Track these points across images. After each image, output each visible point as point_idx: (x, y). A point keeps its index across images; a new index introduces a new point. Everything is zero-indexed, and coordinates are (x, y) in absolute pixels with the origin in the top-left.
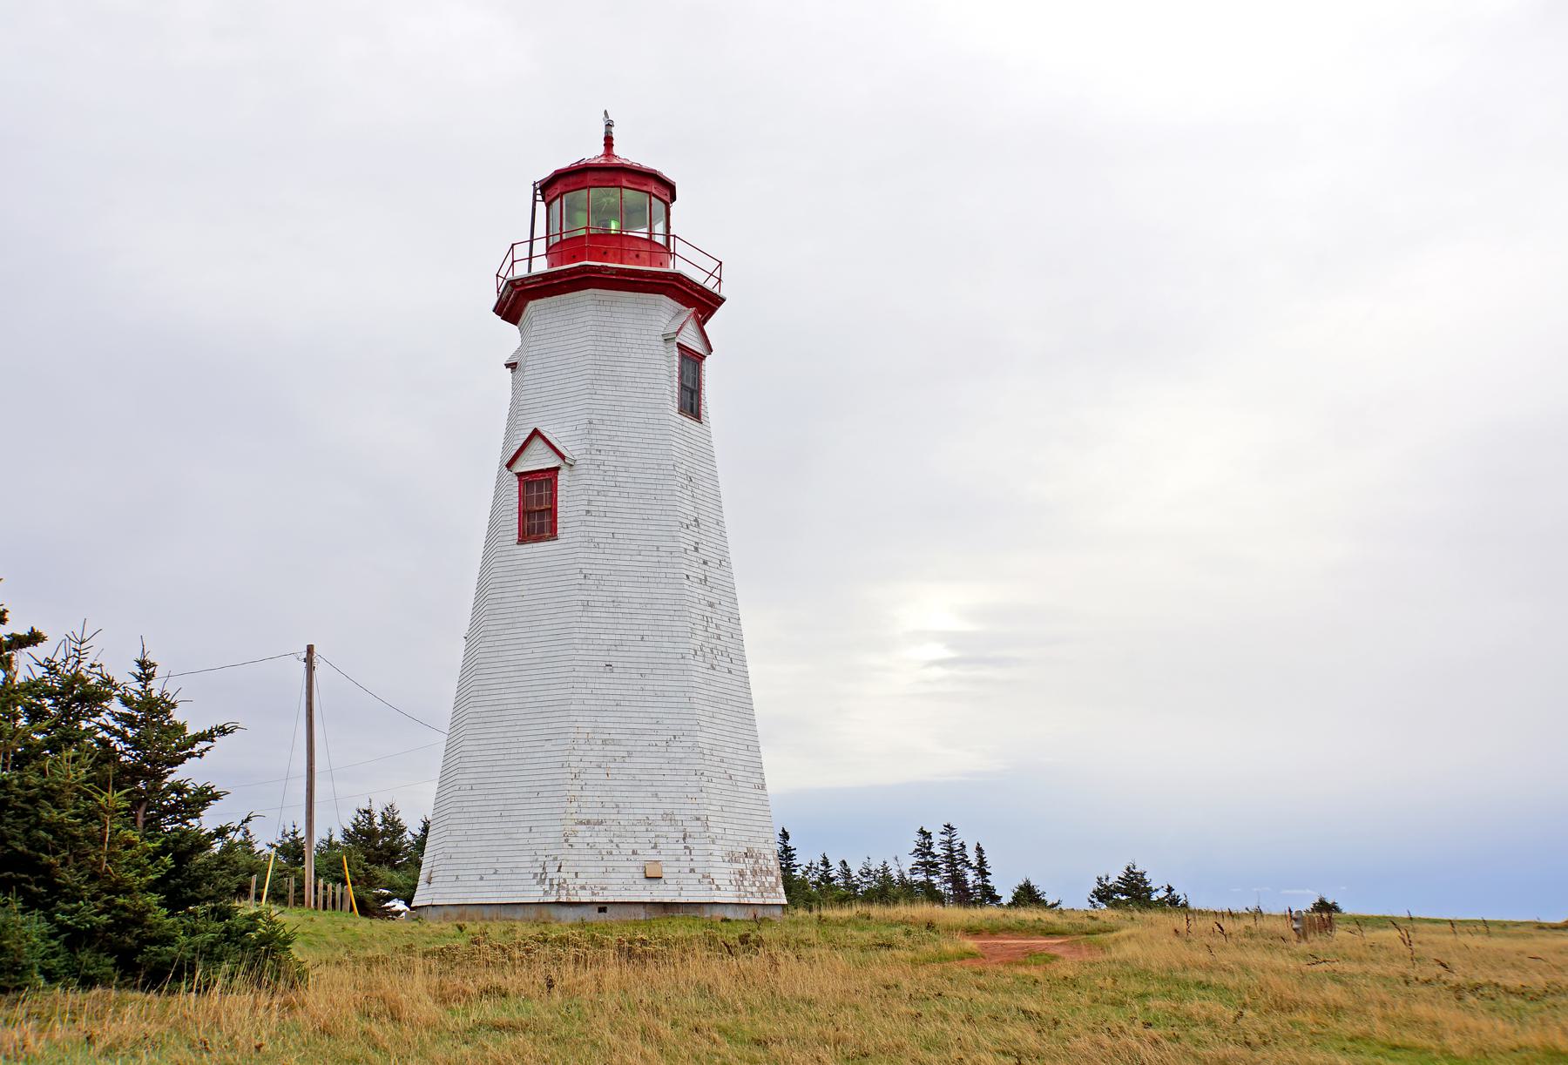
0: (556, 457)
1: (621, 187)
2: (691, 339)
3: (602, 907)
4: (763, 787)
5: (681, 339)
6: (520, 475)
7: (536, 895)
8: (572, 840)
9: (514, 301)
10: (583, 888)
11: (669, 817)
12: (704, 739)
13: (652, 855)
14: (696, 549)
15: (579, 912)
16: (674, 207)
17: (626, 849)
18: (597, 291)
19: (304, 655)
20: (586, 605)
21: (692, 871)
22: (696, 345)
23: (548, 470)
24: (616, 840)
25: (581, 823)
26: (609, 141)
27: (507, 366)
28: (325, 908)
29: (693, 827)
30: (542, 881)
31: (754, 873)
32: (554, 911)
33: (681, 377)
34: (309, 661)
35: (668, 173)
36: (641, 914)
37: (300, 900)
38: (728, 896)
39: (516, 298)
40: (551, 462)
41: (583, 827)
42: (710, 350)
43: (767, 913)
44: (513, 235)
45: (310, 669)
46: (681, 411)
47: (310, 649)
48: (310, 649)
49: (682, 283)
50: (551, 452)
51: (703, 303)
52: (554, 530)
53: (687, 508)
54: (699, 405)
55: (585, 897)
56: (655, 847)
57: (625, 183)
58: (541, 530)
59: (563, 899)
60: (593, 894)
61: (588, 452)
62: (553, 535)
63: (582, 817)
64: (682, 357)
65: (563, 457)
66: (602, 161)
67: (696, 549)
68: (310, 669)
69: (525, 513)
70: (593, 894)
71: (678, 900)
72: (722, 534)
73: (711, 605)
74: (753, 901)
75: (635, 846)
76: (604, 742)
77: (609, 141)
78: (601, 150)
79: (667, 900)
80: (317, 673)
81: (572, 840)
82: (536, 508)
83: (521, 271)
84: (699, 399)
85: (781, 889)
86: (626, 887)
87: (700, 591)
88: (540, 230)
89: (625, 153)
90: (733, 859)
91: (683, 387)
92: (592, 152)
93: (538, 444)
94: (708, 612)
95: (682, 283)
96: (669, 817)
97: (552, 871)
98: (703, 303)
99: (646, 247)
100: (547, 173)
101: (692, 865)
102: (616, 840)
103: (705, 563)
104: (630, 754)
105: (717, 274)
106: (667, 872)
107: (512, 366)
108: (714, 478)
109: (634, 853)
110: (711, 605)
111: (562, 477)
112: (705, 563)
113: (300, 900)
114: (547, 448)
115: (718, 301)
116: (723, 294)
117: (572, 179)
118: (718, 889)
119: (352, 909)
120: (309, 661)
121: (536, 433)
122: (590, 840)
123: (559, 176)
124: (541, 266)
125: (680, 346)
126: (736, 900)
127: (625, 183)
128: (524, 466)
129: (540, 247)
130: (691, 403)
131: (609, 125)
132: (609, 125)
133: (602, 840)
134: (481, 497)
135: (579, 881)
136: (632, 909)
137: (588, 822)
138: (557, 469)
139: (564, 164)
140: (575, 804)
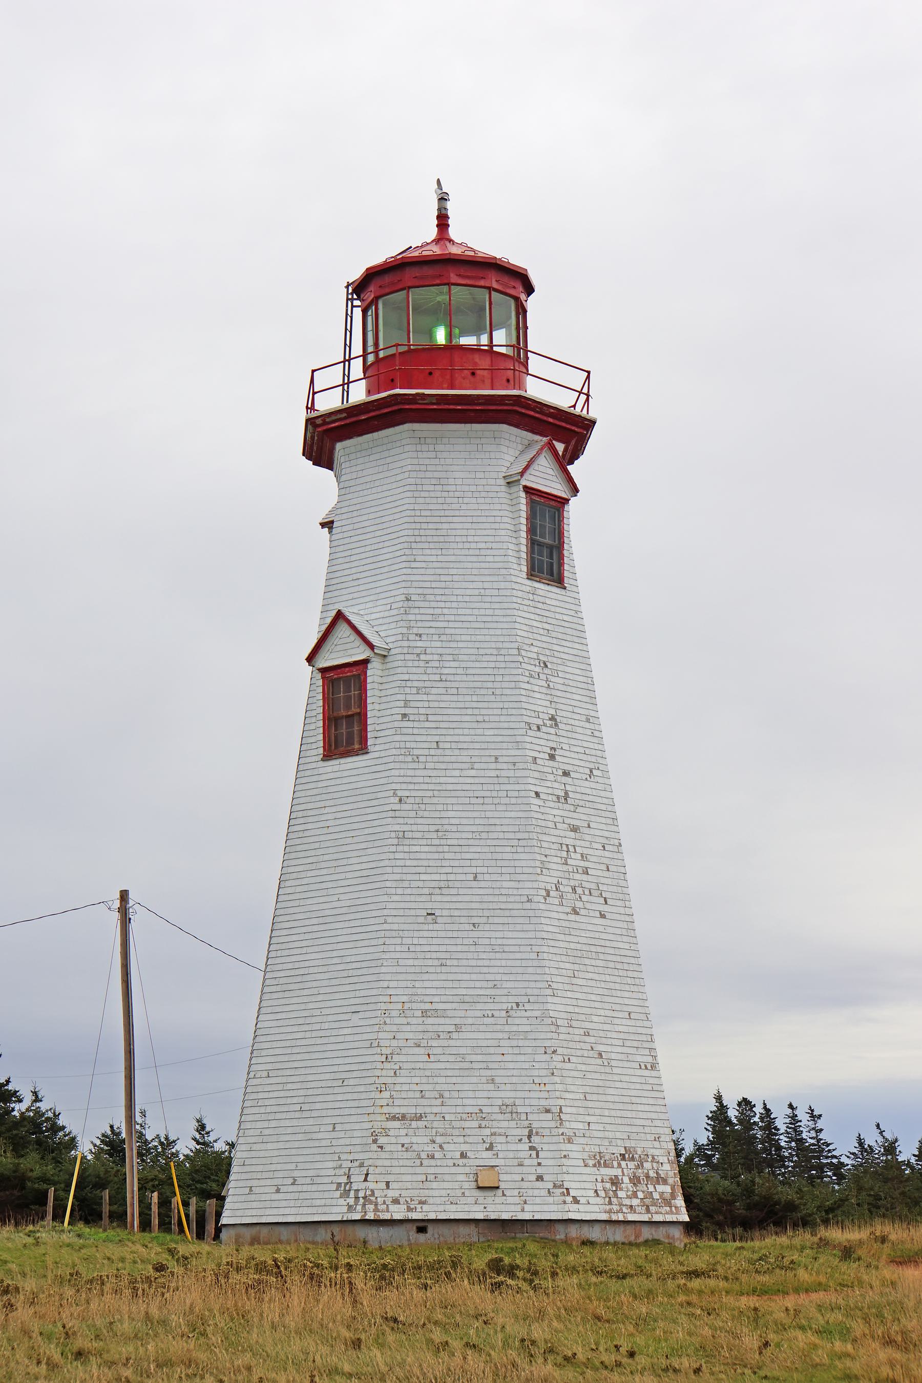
0: (364, 647)
1: (449, 284)
2: (545, 477)
3: (422, 1227)
4: (654, 1067)
5: (529, 480)
6: (323, 671)
7: (338, 1212)
8: (382, 1140)
9: (324, 439)
10: (396, 1201)
11: (509, 1110)
12: (557, 1007)
13: (487, 1158)
14: (552, 757)
15: (384, 1232)
16: (532, 303)
17: (454, 1150)
18: (416, 426)
19: (117, 904)
20: (402, 836)
21: (540, 1178)
22: (557, 488)
23: (356, 663)
24: (439, 1140)
25: (394, 1118)
26: (443, 221)
27: (323, 525)
28: (145, 1225)
29: (542, 1122)
30: (346, 1194)
31: (635, 1180)
32: (362, 1232)
33: (531, 531)
34: (124, 911)
35: (516, 260)
36: (472, 1230)
37: (119, 1217)
38: (593, 1210)
39: (321, 440)
40: (361, 653)
41: (396, 1124)
42: (575, 490)
43: (660, 1234)
44: (317, 350)
45: (125, 921)
46: (531, 575)
47: (124, 896)
48: (124, 896)
49: (528, 407)
50: (359, 641)
51: (567, 432)
52: (364, 740)
53: (541, 705)
54: (561, 564)
55: (398, 1212)
56: (490, 1148)
57: (454, 278)
58: (350, 741)
59: (370, 1216)
60: (409, 1209)
61: (405, 637)
62: (363, 749)
63: (396, 1110)
64: (531, 505)
65: (371, 646)
66: (436, 250)
67: (552, 757)
68: (125, 921)
69: (331, 720)
70: (409, 1209)
71: (521, 1216)
72: (595, 734)
73: (575, 829)
74: (631, 1217)
75: (464, 1148)
76: (425, 1013)
77: (443, 221)
78: (432, 232)
79: (505, 1216)
80: (134, 926)
81: (382, 1140)
82: (343, 714)
83: (328, 402)
84: (561, 557)
85: (680, 1202)
86: (450, 1198)
87: (555, 811)
88: (357, 349)
89: (473, 235)
90: (601, 1162)
91: (533, 543)
92: (418, 234)
93: (343, 630)
94: (570, 838)
95: (528, 407)
96: (509, 1110)
97: (357, 1178)
98: (567, 432)
99: (484, 362)
100: (356, 274)
101: (540, 1170)
102: (439, 1140)
103: (566, 774)
104: (458, 1028)
105: (585, 390)
106: (506, 1180)
107: (328, 525)
108: (584, 660)
109: (463, 1155)
110: (575, 829)
111: (374, 672)
112: (566, 774)
113: (119, 1217)
114: (354, 636)
115: (590, 424)
116: (592, 415)
117: (387, 279)
118: (576, 1201)
119: (182, 1231)
120: (124, 911)
121: (340, 616)
122: (406, 1140)
123: (372, 275)
124: (359, 394)
125: (527, 489)
126: (604, 1217)
127: (454, 278)
128: (327, 660)
129: (357, 368)
130: (547, 559)
131: (443, 199)
132: (443, 199)
133: (420, 1141)
134: (296, 694)
135: (392, 1194)
136: (454, 1227)
137: (404, 1117)
138: (365, 662)
139: (378, 258)
140: (386, 1094)
